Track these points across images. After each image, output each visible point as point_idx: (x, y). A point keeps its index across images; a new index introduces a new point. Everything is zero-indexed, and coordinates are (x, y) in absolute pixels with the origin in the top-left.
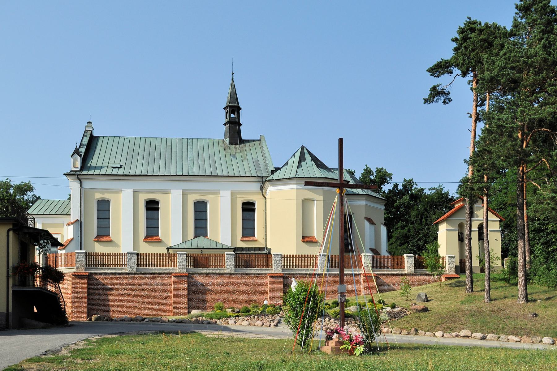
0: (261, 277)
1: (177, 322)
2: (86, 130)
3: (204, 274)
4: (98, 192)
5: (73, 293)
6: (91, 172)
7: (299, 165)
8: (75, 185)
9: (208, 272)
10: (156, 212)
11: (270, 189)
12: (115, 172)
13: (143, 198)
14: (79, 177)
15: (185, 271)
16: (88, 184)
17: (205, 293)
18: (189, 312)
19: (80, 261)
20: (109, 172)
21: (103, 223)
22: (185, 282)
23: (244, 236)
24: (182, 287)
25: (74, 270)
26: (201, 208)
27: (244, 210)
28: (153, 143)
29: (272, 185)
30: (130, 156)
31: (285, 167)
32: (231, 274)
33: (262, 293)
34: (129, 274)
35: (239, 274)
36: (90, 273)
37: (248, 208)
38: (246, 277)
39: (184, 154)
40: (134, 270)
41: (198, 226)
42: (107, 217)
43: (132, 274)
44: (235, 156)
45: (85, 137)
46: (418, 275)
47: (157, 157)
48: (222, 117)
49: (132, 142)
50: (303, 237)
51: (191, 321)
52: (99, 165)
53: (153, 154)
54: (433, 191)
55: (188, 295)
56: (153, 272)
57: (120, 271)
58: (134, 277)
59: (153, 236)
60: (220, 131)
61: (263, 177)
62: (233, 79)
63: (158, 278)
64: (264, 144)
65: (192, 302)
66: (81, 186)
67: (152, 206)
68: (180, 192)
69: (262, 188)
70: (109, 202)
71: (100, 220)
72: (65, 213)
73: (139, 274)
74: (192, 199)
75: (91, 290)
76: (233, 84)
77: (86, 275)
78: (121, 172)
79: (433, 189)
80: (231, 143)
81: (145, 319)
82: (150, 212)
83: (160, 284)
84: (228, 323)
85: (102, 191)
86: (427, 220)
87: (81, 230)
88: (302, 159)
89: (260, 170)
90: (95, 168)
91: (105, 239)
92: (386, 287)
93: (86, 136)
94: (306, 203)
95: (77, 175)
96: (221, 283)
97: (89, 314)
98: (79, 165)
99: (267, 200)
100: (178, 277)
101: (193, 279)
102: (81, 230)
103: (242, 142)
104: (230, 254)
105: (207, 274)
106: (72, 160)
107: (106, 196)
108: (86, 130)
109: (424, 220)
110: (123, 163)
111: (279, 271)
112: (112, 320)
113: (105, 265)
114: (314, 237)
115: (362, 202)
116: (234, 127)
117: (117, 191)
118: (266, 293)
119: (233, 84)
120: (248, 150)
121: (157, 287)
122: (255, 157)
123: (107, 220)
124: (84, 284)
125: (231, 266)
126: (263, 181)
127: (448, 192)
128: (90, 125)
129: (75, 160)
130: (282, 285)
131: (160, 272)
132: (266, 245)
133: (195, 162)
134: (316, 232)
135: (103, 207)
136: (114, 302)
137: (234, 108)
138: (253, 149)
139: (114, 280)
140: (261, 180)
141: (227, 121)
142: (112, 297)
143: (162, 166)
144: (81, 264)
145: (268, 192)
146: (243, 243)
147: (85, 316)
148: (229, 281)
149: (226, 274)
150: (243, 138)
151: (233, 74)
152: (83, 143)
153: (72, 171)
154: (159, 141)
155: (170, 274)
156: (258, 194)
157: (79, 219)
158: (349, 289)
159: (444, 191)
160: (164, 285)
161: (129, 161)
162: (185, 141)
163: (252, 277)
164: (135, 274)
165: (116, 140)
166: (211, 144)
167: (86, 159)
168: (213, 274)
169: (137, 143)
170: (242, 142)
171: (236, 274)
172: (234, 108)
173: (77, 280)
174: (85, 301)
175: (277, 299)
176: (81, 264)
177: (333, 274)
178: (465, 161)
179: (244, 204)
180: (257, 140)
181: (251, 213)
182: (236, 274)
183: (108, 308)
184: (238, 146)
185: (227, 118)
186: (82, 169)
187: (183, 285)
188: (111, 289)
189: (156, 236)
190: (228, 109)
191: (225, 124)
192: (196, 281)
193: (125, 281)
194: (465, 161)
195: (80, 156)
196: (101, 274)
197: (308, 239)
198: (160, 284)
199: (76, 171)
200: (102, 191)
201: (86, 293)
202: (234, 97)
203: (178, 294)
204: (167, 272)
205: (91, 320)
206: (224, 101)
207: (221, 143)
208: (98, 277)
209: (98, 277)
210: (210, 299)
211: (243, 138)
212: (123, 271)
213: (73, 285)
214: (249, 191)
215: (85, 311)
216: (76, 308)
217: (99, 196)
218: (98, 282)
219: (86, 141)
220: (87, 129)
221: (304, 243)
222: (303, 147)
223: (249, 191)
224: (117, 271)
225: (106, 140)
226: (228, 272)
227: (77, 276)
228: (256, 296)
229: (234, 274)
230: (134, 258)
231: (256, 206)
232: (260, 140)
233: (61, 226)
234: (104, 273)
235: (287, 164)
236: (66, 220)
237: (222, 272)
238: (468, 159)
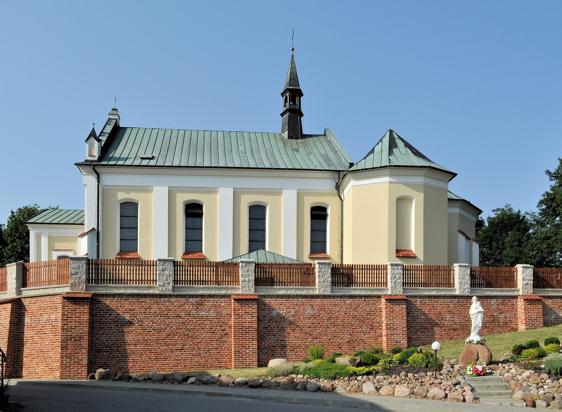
0: (372, 301)
1: (252, 387)
2: (109, 119)
3: (282, 296)
5: (63, 329)
6: (111, 163)
7: (390, 152)
8: (90, 180)
9: (289, 292)
10: (198, 219)
11: (351, 186)
12: (145, 162)
13: (182, 199)
14: (98, 169)
15: (252, 292)
16: (111, 179)
17: (283, 329)
18: (262, 363)
19: (76, 273)
20: (137, 162)
21: (129, 234)
22: (253, 309)
23: (313, 251)
24: (248, 318)
25: (68, 290)
26: (257, 214)
27: (313, 217)
28: (194, 136)
29: (357, 179)
30: (165, 148)
31: (371, 155)
32: (325, 297)
33: (372, 328)
34: (160, 296)
35: (338, 297)
36: (95, 295)
37: (319, 214)
38: (349, 301)
39: (234, 148)
40: (169, 289)
41: (253, 239)
42: (134, 226)
43: (165, 296)
44: (297, 150)
45: (107, 126)
46: (177, 296)
47: (200, 149)
48: (280, 105)
49: (168, 134)
50: (398, 251)
51: (278, 385)
52: (124, 155)
53: (195, 146)
54: (499, 212)
55: (258, 330)
56: (201, 292)
57: (146, 292)
58: (169, 301)
59: (194, 253)
60: (277, 123)
61: (339, 171)
62: (293, 56)
63: (209, 303)
64: (332, 137)
65: (265, 344)
66: (98, 182)
67: (194, 211)
69: (338, 187)
70: (137, 204)
71: (124, 230)
72: (79, 222)
73: (177, 296)
75: (97, 325)
76: (293, 62)
77: (87, 298)
78: (152, 163)
79: (498, 210)
80: (290, 137)
81: (188, 378)
82: (190, 219)
83: (212, 313)
84: (359, 389)
85: (128, 189)
86: (497, 243)
87: (98, 242)
88: (392, 145)
89: (333, 165)
90: (119, 159)
91: (131, 256)
92: (553, 317)
93: (110, 124)
94: (401, 203)
95: (94, 166)
96: (309, 311)
97: (91, 367)
98: (96, 153)
99: (344, 203)
100: (242, 301)
101: (265, 304)
102: (98, 242)
103: (304, 136)
104: (324, 263)
105: (288, 297)
106: (87, 146)
107: (133, 196)
108: (109, 119)
109: (494, 244)
110: (155, 154)
111: (399, 291)
112: (130, 378)
113: (120, 281)
114: (411, 251)
116: (294, 115)
117: (147, 190)
118: (380, 327)
119: (293, 62)
120: (312, 145)
122: (322, 151)
123: (134, 230)
124: (83, 313)
125: (325, 284)
126: (340, 176)
127: (519, 212)
128: (115, 112)
129: (91, 146)
130: (405, 314)
131: (213, 292)
132: (342, 261)
133: (249, 156)
134: (415, 244)
135: (129, 211)
136: (135, 345)
137: (294, 94)
138: (319, 145)
139: (137, 306)
140: (336, 175)
141: (285, 109)
142: (130, 337)
143: (207, 155)
144: (80, 278)
145: (346, 191)
147: (85, 369)
148: (322, 308)
149: (317, 297)
150: (304, 132)
151: (293, 50)
152: (105, 131)
153: (86, 161)
154: (201, 134)
155: (229, 296)
156: (332, 195)
157: (96, 228)
158: (501, 320)
159: (515, 211)
160: (219, 316)
161: (163, 153)
162: (233, 135)
163: (357, 301)
164: (170, 296)
165: (148, 132)
166: (265, 138)
167: (105, 151)
168: (297, 296)
169: (174, 134)
170: (304, 136)
171: (334, 297)
172: (294, 94)
173: (71, 306)
174: (85, 343)
175: (398, 338)
176: (80, 278)
178: (548, 172)
179: (313, 209)
180: (321, 135)
181: (322, 221)
182: (334, 297)
183: (124, 356)
184: (299, 141)
185: (285, 106)
186: (101, 158)
187: (250, 316)
188: (131, 323)
189: (198, 252)
190: (288, 94)
191: (282, 115)
192: (270, 309)
193: (155, 308)
194: (548, 172)
195: (99, 140)
196: (114, 295)
197: (403, 253)
198: (212, 313)
199: (93, 161)
200: (128, 189)
201: (86, 329)
202: (294, 78)
203: (241, 330)
204: (223, 292)
205: (93, 377)
206: (282, 84)
207: (278, 137)
208: (108, 302)
209: (108, 302)
210: (292, 338)
211: (304, 132)
212: (151, 291)
213: (63, 315)
214: (320, 191)
215: (85, 362)
216: (69, 356)
217: (122, 196)
218: (108, 310)
219: (109, 129)
220: (111, 117)
222: (391, 132)
223: (320, 191)
224: (141, 292)
225: (134, 131)
226: (321, 292)
228: (365, 333)
229: (329, 296)
230: (170, 268)
231: (329, 212)
232: (325, 135)
233: (74, 239)
234: (120, 295)
235: (372, 151)
236: (79, 230)
237: (310, 293)
238: (553, 171)
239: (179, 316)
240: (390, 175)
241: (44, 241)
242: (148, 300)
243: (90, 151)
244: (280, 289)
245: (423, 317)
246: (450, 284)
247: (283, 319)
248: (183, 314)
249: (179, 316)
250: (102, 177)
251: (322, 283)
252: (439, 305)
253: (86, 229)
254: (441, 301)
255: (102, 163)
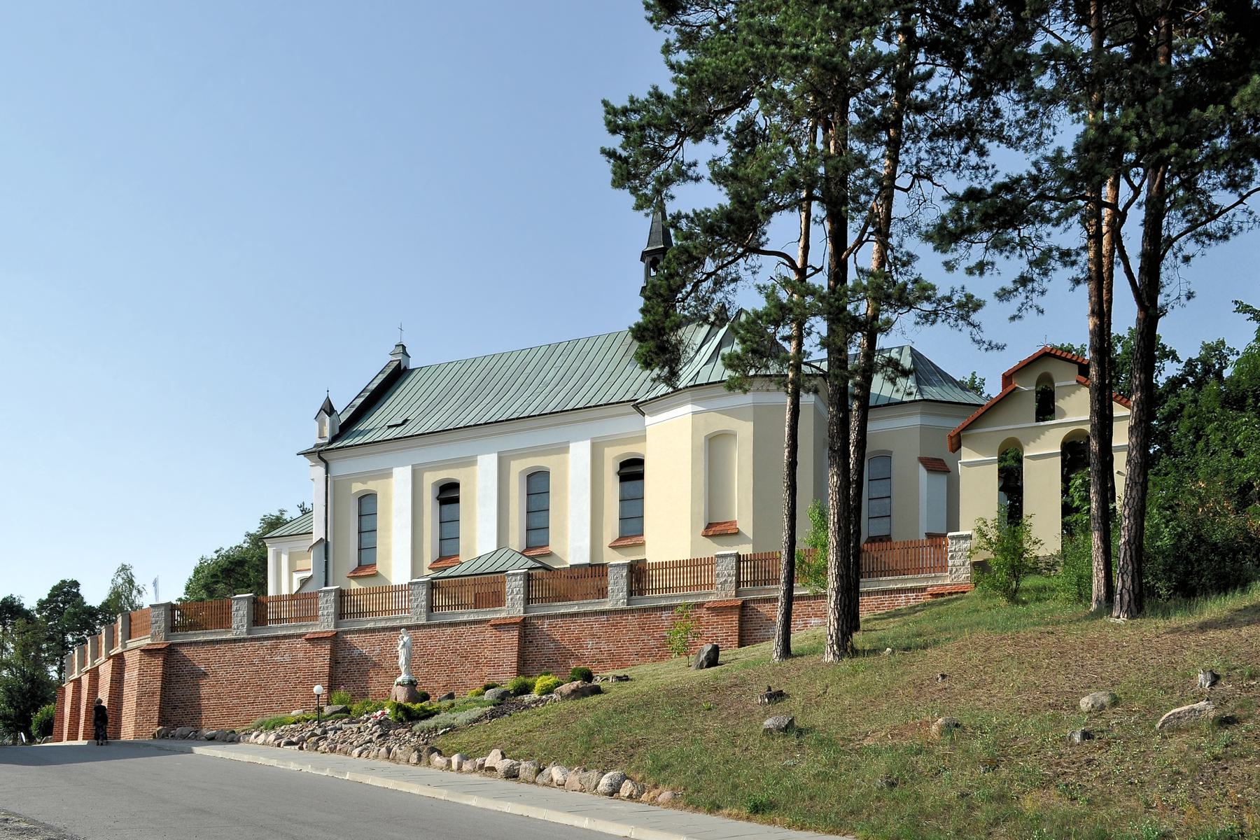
4: (357, 480)
12: (395, 433)
13: (431, 479)
15: (332, 628)
22: (325, 650)
25: (149, 641)
27: (624, 478)
34: (235, 641)
38: (449, 631)
43: (240, 640)
46: (439, 625)
63: (284, 645)
68: (495, 456)
74: (518, 468)
75: (174, 678)
87: (326, 558)
91: (368, 572)
95: (319, 454)
101: (345, 643)
102: (326, 558)
107: (371, 486)
115: (913, 421)
121: (281, 664)
134: (741, 512)
135: (367, 504)
146: (615, 553)
164: (244, 640)
171: (429, 626)
173: (147, 659)
174: (157, 699)
177: (639, 609)
182: (429, 626)
192: (352, 647)
197: (718, 528)
198: (287, 658)
201: (159, 684)
209: (184, 651)
217: (357, 487)
218: (185, 660)
221: (708, 541)
227: (148, 652)
229: (423, 626)
234: (196, 643)
239: (252, 664)
240: (694, 402)
241: (285, 559)
242: (223, 647)
243: (321, 431)
244: (369, 621)
245: (552, 645)
246: (602, 593)
247: (366, 659)
248: (256, 661)
249: (252, 664)
250: (332, 465)
251: (617, 588)
252: (575, 627)
253: (315, 538)
254: (580, 620)
255: (346, 443)
